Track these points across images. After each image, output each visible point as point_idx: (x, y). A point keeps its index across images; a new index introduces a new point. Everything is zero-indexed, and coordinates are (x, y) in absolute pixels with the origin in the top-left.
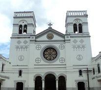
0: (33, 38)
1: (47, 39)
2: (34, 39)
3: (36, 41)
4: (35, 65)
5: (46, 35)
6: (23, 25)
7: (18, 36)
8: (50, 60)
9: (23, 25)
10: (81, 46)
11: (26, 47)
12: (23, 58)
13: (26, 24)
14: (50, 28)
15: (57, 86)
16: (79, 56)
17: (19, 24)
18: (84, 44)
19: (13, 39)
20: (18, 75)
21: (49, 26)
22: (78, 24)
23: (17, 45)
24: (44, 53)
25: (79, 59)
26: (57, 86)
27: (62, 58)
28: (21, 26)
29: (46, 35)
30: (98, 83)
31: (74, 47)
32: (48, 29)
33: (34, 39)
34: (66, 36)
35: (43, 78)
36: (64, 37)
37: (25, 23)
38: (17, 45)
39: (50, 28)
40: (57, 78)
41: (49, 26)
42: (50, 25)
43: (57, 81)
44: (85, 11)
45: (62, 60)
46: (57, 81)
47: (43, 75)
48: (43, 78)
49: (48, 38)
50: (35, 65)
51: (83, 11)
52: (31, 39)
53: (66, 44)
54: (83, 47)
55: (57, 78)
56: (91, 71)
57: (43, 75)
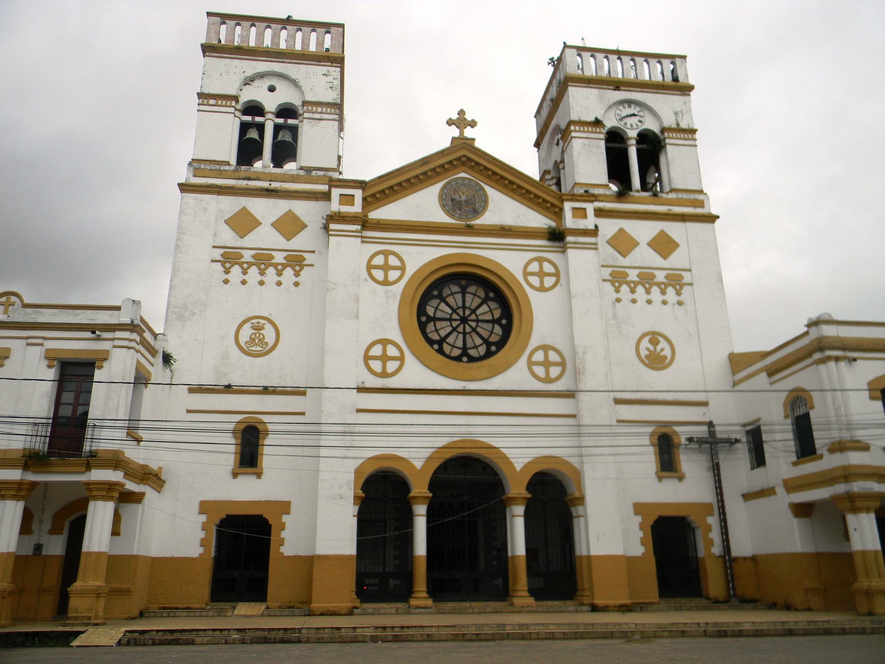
0: (347, 200)
1: (441, 217)
2: (357, 208)
3: (366, 224)
4: (361, 390)
5: (438, 187)
6: (271, 103)
7: (234, 176)
8: (465, 356)
9: (271, 103)
10: (279, 258)
11: (296, 261)
12: (269, 334)
13: (297, 102)
14: (463, 145)
15: (421, 548)
16: (654, 337)
17: (610, 122)
18: (677, 260)
19: (190, 197)
20: (228, 455)
21: (455, 132)
22: (633, 134)
23: (228, 237)
24: (421, 310)
25: (656, 362)
26: (421, 548)
27: (546, 348)
28: (254, 109)
29: (438, 187)
30: (795, 524)
31: (618, 278)
32: (442, 153)
33: (357, 208)
34: (568, 206)
35: (420, 488)
36: (557, 212)
37: (285, 95)
38: (228, 237)
39: (463, 145)
40: (516, 488)
41: (455, 132)
42: (461, 121)
43: (420, 511)
44: (327, 26)
45: (547, 364)
46: (420, 511)
47: (418, 464)
48: (420, 488)
49: (449, 213)
50: (361, 390)
51: (314, 25)
52: (335, 206)
53: (573, 254)
54: (676, 281)
55: (516, 488)
56: (732, 442)
57: (418, 464)
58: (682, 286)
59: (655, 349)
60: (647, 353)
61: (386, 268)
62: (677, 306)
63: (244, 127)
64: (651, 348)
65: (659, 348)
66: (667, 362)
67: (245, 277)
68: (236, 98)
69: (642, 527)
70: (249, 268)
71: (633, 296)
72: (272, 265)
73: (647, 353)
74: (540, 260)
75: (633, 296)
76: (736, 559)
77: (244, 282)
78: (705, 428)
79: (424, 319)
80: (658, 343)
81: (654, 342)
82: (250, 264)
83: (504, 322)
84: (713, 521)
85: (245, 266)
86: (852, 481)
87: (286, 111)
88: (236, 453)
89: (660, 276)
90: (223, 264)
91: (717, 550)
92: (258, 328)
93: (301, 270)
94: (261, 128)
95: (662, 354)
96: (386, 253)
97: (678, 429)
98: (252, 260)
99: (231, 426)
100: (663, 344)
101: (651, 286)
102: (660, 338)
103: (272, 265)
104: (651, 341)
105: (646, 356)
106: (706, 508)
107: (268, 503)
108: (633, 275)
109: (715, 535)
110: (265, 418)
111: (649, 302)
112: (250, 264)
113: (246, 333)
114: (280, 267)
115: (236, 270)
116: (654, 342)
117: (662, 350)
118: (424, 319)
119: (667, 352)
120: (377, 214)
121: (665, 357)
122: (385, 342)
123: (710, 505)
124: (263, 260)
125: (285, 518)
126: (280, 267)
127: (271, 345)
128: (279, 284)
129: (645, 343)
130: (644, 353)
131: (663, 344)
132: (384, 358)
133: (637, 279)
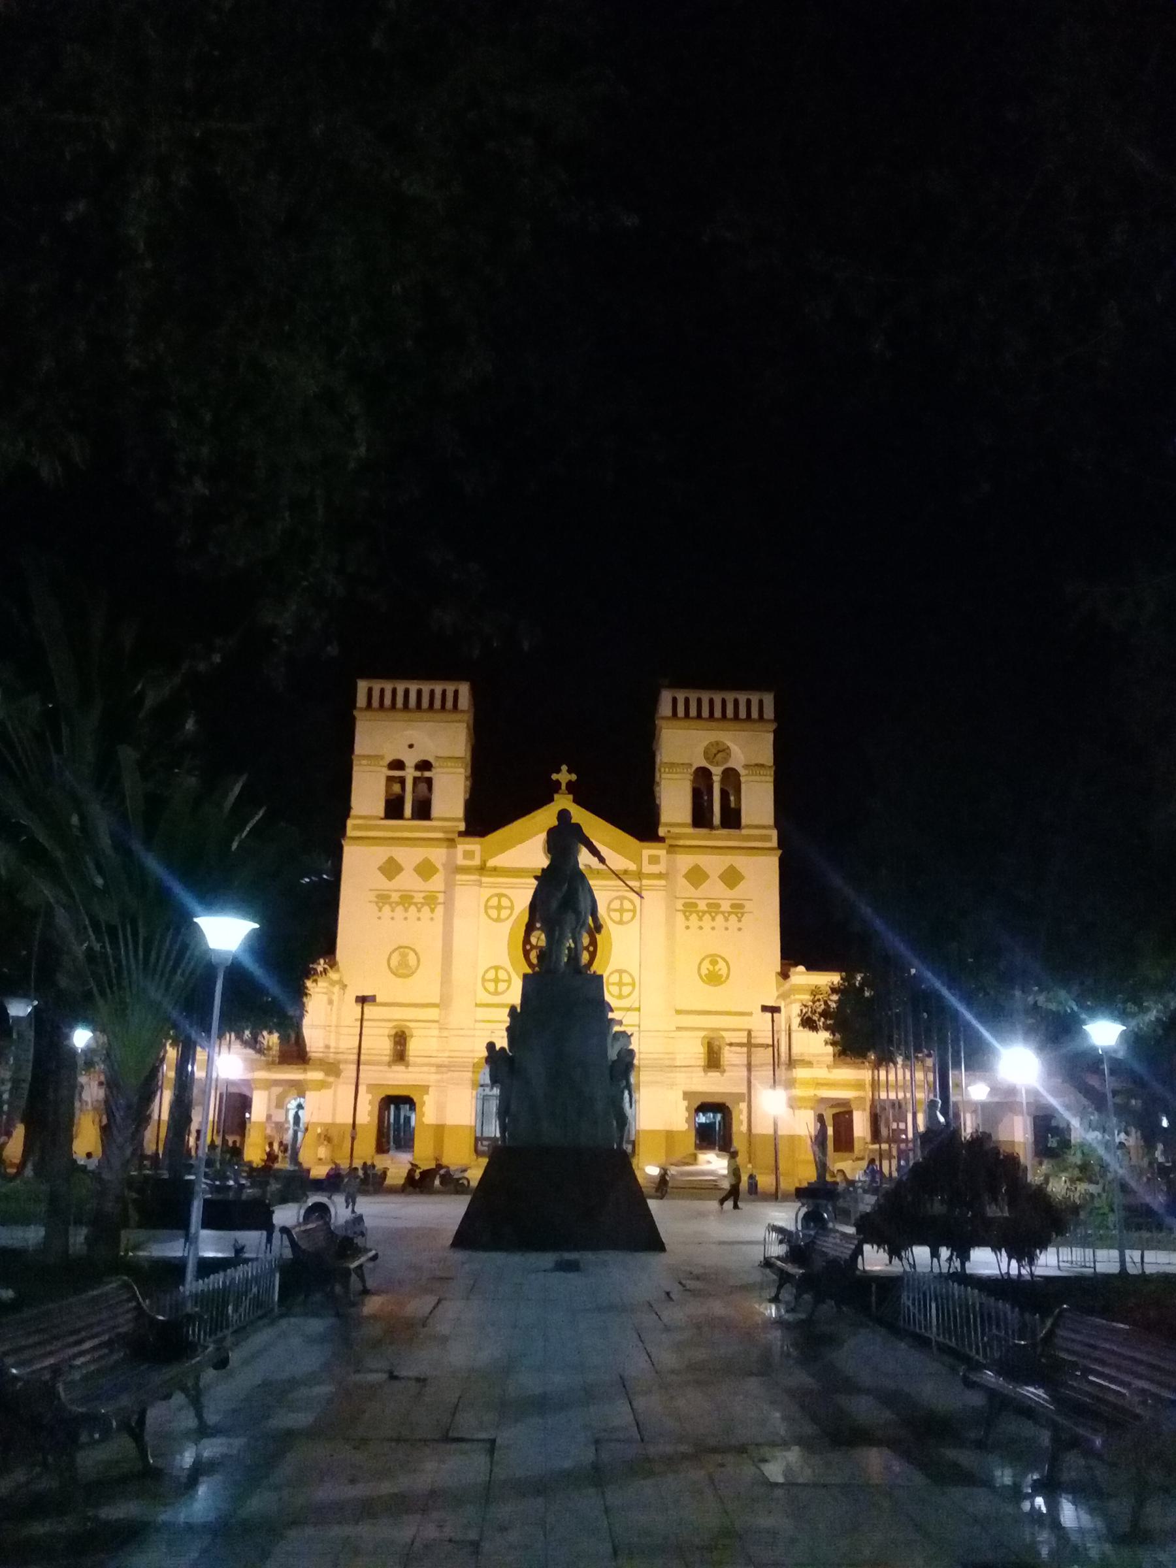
23: (382, 883)
58: (743, 914)
60: (707, 972)
61: (499, 907)
64: (711, 968)
65: (717, 968)
66: (723, 979)
70: (422, 907)
71: (380, 914)
73: (707, 972)
74: (621, 898)
80: (717, 962)
81: (714, 963)
82: (704, 913)
83: (591, 949)
84: (743, 1106)
85: (394, 905)
88: (704, 1058)
89: (419, 898)
91: (744, 1128)
95: (719, 973)
96: (500, 896)
97: (723, 1034)
99: (386, 1032)
100: (722, 964)
101: (717, 913)
102: (719, 959)
105: (706, 975)
107: (731, 1094)
108: (395, 897)
109: (744, 1117)
110: (408, 1024)
111: (701, 928)
112: (704, 913)
113: (706, 965)
114: (419, 906)
115: (387, 908)
116: (714, 963)
117: (720, 969)
118: (528, 947)
119: (724, 972)
120: (491, 863)
121: (721, 976)
124: (406, 900)
125: (426, 1098)
126: (394, 905)
127: (414, 968)
129: (706, 965)
130: (704, 971)
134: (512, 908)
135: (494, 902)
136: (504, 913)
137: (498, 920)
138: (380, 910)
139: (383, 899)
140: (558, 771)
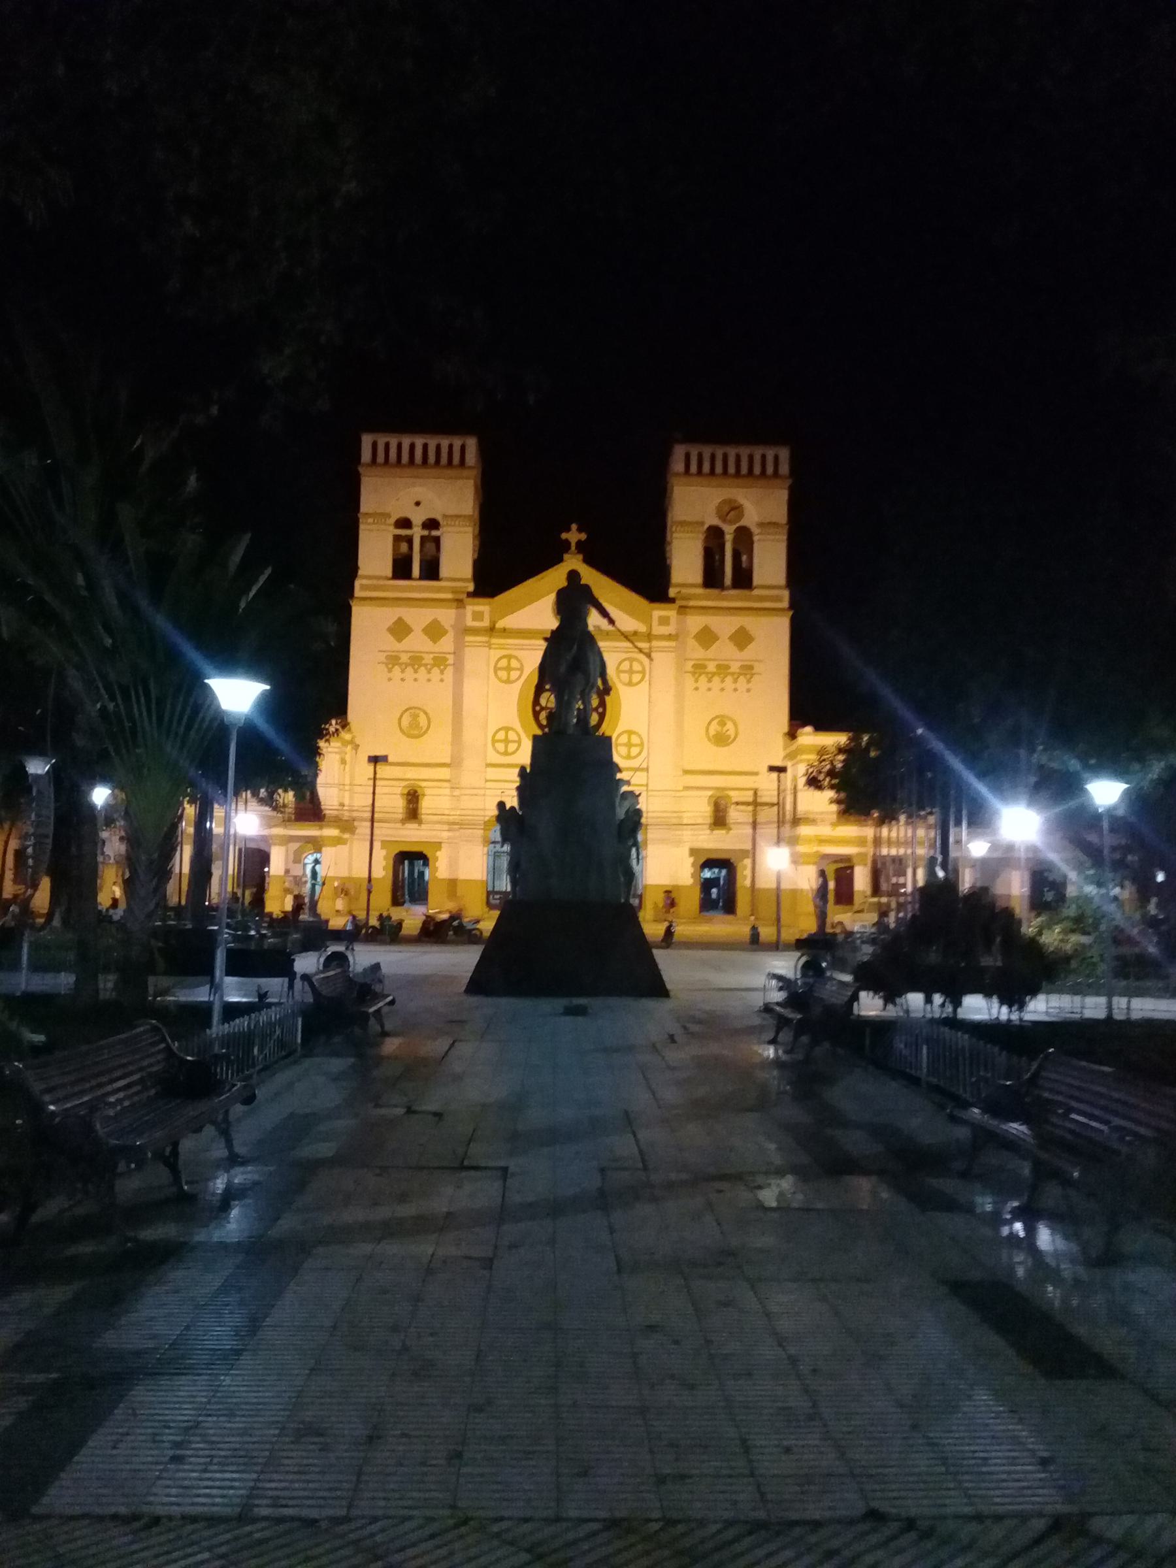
6: (418, 518)
9: (418, 518)
12: (422, 720)
28: (405, 523)
59: (722, 729)
62: (440, 683)
63: (397, 539)
64: (719, 729)
65: (725, 729)
67: (723, 685)
68: (702, 523)
69: (385, 858)
72: (729, 674)
75: (416, 676)
76: (759, 890)
77: (442, 680)
78: (751, 793)
79: (600, 710)
82: (714, 674)
86: (855, 837)
87: (432, 524)
89: (428, 659)
90: (387, 664)
91: (748, 883)
92: (415, 717)
93: (751, 678)
94: (409, 540)
97: (731, 793)
98: (409, 661)
101: (420, 666)
103: (729, 674)
104: (719, 723)
106: (744, 853)
107: (734, 851)
109: (748, 872)
110: (424, 784)
113: (406, 721)
119: (732, 733)
121: (729, 737)
122: (507, 729)
123: (747, 851)
126: (429, 667)
127: (424, 729)
128: (442, 680)
129: (714, 724)
130: (712, 732)
131: (730, 725)
132: (506, 741)
133: (715, 670)
134: (521, 669)
135: (504, 663)
136: (514, 675)
137: (508, 681)
138: (696, 681)
139: (393, 660)
140: (568, 530)
